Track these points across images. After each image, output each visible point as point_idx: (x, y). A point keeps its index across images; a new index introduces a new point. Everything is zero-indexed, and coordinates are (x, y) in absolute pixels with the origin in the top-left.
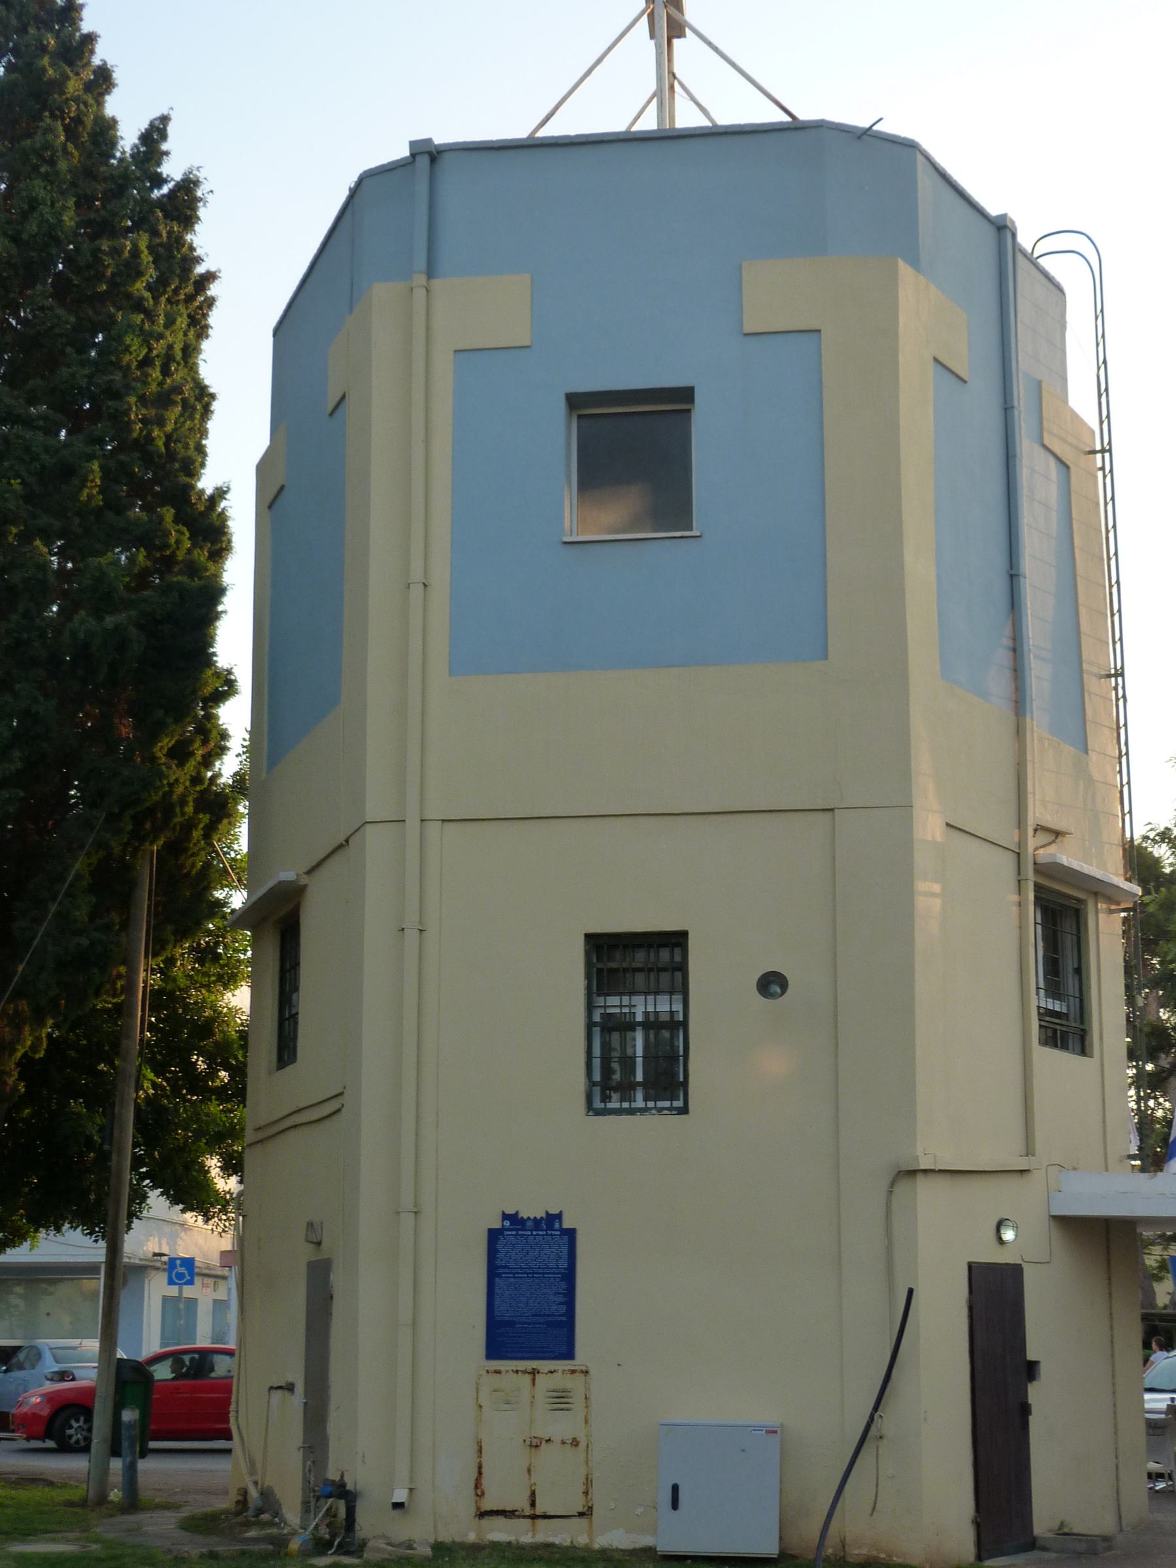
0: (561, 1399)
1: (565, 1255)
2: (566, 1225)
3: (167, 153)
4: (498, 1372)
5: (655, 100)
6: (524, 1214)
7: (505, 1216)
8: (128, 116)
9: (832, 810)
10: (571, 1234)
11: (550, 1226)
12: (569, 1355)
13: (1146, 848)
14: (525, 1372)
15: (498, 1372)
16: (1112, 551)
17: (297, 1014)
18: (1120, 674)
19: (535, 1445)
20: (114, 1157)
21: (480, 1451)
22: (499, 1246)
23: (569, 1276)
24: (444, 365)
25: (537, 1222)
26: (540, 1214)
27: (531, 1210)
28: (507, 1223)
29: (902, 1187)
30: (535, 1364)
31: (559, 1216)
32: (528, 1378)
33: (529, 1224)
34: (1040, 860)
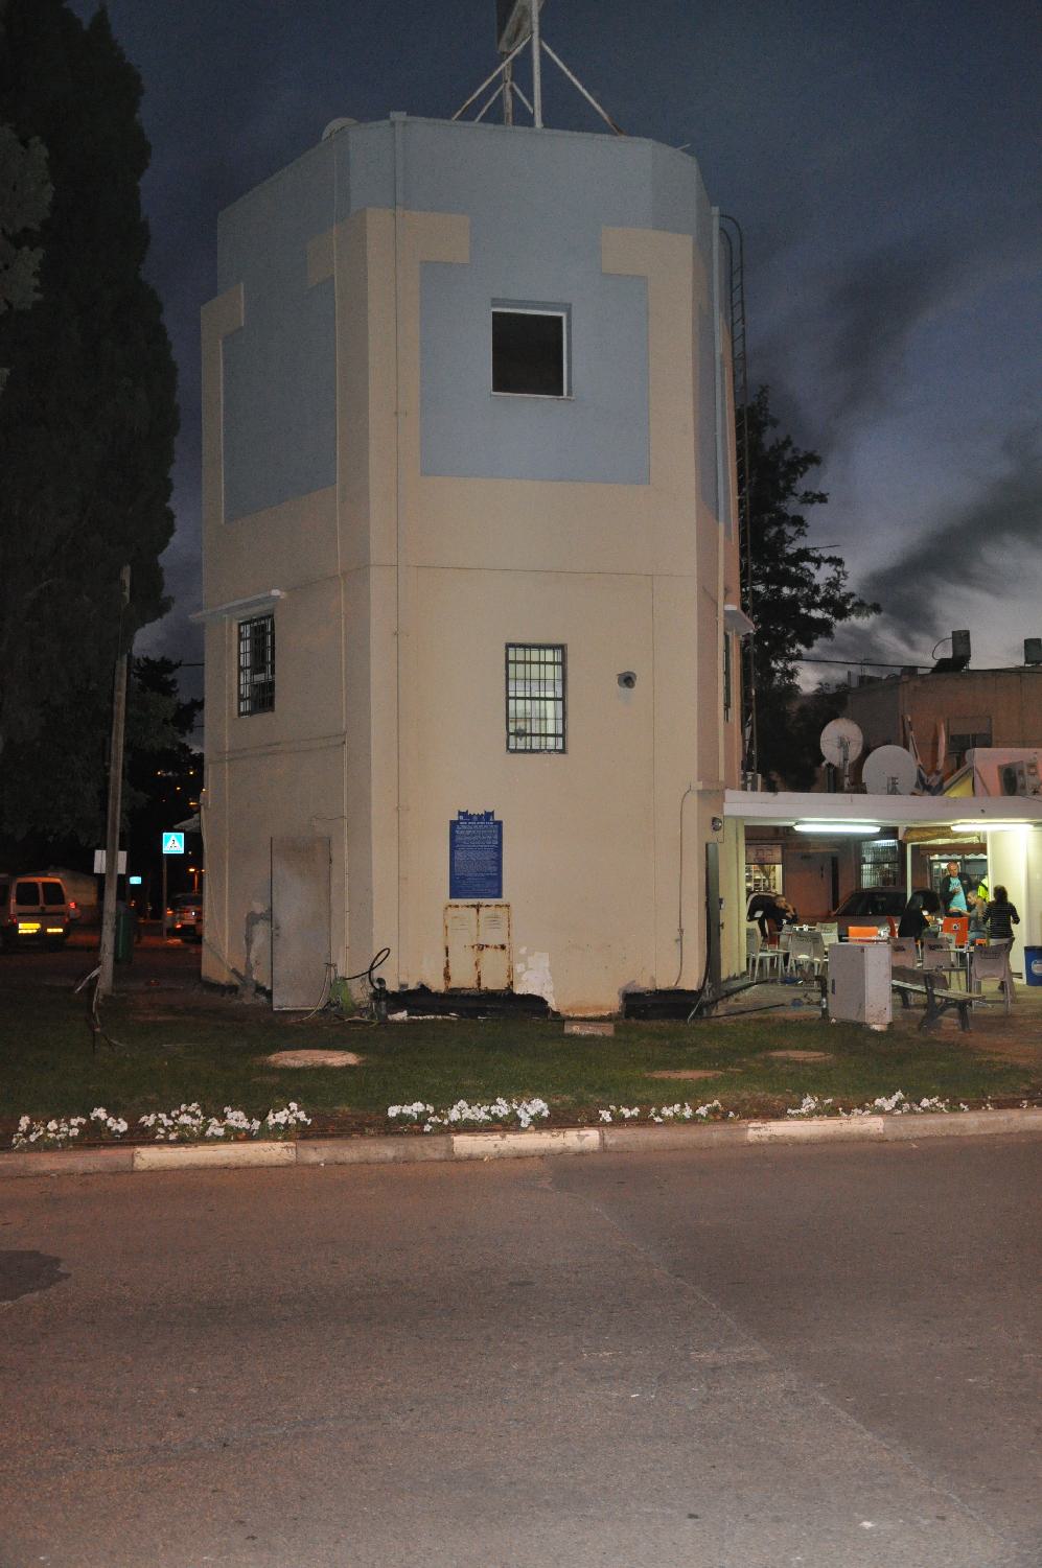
2: (497, 818)
3: (101, 22)
4: (457, 906)
6: (471, 812)
7: (460, 813)
10: (499, 824)
11: (488, 820)
12: (499, 895)
14: (473, 906)
15: (457, 906)
17: (199, 705)
18: (203, 664)
19: (481, 947)
20: (112, 769)
21: (447, 952)
23: (499, 849)
24: (861, 944)
25: (480, 817)
26: (481, 812)
27: (476, 809)
28: (461, 818)
30: (481, 901)
31: (492, 813)
32: (474, 910)
33: (475, 818)
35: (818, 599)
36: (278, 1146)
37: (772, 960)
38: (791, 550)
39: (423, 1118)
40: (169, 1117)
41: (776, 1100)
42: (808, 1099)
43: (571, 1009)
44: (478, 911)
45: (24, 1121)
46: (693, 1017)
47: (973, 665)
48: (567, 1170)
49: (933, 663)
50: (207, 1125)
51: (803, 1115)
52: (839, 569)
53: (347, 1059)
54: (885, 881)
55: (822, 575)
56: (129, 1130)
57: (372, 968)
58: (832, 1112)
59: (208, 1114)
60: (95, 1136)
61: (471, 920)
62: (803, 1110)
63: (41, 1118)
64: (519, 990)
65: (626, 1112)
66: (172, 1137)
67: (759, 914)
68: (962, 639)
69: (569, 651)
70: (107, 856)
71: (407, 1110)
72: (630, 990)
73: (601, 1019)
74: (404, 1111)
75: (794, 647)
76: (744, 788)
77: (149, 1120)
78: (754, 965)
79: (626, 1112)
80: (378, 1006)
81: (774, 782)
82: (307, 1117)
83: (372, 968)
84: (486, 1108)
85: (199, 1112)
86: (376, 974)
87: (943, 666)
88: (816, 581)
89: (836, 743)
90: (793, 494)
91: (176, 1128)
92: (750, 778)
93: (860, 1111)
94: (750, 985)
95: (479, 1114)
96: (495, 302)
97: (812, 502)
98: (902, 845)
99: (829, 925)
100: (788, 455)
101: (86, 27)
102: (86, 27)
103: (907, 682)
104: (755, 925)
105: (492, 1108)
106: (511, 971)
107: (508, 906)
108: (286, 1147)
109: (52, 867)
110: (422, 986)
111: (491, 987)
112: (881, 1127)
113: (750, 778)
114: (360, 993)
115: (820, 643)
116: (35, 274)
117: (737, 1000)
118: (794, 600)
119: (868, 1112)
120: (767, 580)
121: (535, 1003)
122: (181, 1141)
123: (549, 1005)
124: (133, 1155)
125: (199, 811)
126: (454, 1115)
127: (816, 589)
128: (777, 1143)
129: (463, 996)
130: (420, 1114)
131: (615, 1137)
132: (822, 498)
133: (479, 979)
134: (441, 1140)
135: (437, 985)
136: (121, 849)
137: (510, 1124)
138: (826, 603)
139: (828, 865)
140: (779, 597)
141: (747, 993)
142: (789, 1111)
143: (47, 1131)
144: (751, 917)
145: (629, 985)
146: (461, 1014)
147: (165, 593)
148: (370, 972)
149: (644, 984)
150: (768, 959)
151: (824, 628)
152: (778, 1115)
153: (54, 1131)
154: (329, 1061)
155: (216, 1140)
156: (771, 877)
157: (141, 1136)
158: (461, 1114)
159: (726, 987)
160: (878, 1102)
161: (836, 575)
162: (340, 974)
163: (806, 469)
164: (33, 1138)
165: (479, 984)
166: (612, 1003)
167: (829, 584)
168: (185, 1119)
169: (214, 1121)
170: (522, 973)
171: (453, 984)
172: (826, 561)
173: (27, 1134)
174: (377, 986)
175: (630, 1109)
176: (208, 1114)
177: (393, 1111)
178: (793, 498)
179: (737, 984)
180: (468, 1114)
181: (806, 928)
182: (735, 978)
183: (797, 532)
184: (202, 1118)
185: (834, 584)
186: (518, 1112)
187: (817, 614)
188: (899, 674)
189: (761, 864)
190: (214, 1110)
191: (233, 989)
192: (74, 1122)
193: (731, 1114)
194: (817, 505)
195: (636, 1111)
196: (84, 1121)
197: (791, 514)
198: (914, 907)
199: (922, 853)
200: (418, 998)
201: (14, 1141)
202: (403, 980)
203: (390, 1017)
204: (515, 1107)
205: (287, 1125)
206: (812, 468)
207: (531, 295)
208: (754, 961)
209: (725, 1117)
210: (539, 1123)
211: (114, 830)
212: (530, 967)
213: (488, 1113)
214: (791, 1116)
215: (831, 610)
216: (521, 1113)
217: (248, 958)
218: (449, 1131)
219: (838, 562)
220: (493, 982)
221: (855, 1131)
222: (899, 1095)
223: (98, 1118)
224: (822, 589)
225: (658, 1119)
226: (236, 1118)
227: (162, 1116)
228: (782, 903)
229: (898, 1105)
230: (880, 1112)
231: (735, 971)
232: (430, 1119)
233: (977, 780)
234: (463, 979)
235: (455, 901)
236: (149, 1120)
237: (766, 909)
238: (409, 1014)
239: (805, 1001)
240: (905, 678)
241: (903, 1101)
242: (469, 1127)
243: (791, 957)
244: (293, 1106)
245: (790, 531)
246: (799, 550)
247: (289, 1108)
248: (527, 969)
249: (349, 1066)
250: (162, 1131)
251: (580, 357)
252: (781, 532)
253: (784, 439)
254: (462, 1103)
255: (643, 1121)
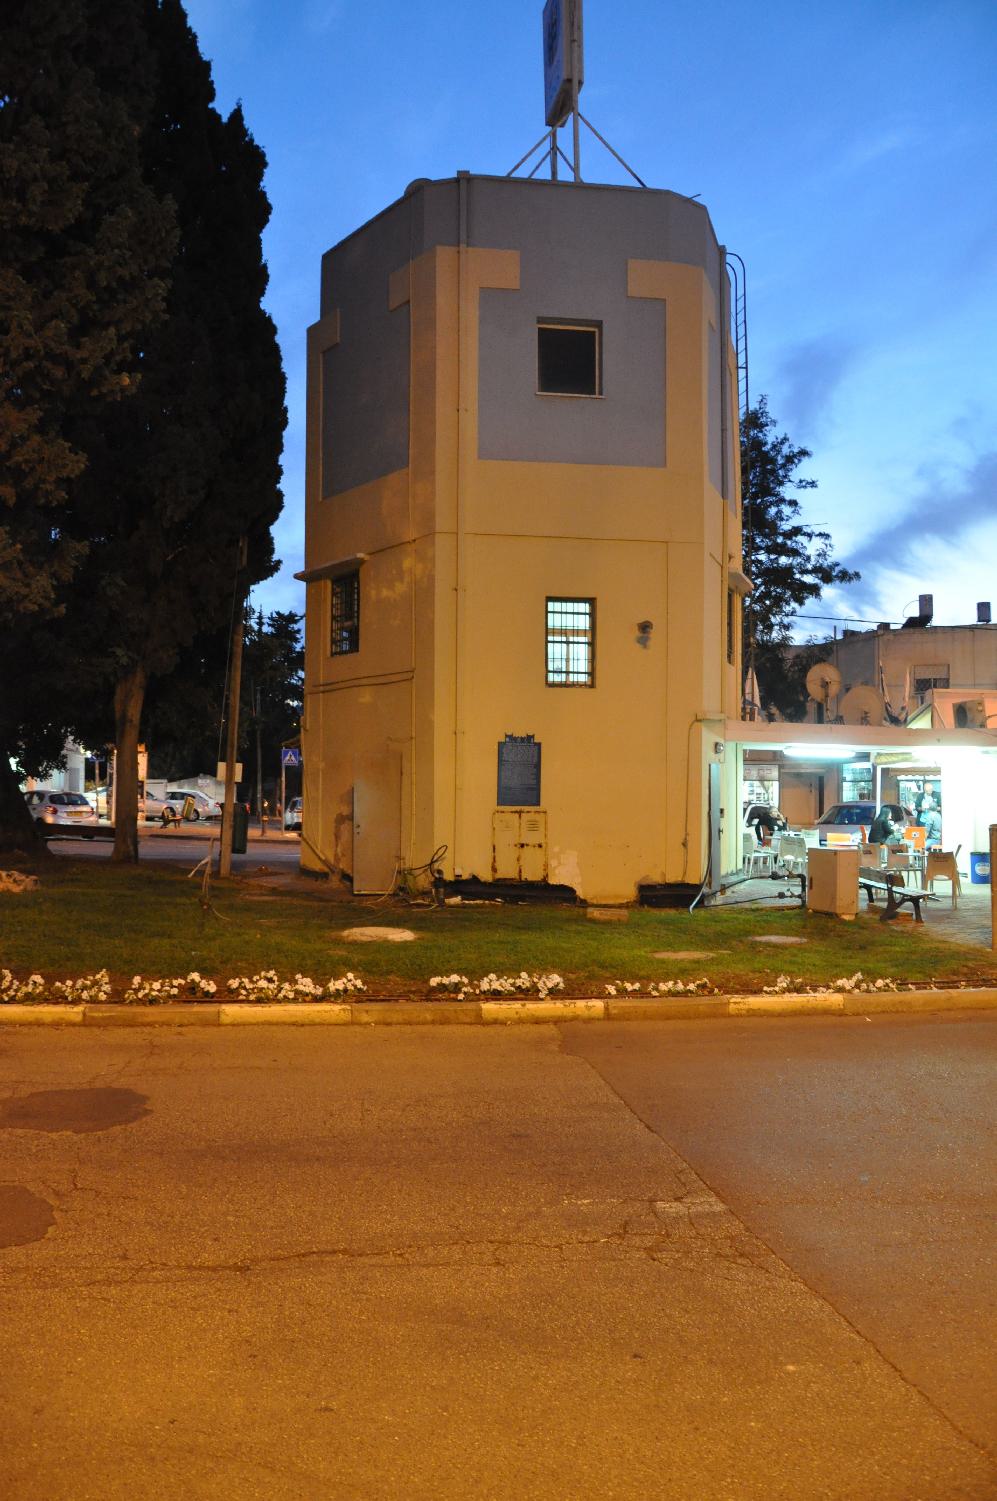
0: (533, 826)
1: (536, 755)
5: (549, 157)
6: (516, 735)
7: (507, 736)
8: (223, 107)
9: (667, 542)
10: (539, 745)
12: (538, 803)
13: (176, 212)
16: (740, 292)
22: (504, 750)
23: (538, 766)
26: (524, 735)
27: (520, 733)
28: (508, 739)
29: (696, 724)
30: (526, 808)
31: (533, 737)
32: (517, 815)
34: (731, 571)
35: (809, 567)
36: (337, 1008)
37: (765, 859)
38: (786, 526)
39: (457, 987)
40: (251, 981)
41: (755, 978)
42: (782, 978)
43: (595, 897)
44: (520, 816)
45: (137, 980)
46: (695, 907)
47: (936, 621)
48: (571, 1036)
49: (904, 621)
50: (280, 989)
51: (777, 993)
52: (827, 542)
53: (404, 935)
54: (862, 796)
55: (812, 548)
56: (217, 992)
57: (432, 862)
58: (799, 990)
59: (282, 980)
60: (191, 994)
61: (514, 823)
62: (777, 989)
63: (148, 977)
64: (552, 881)
65: (629, 987)
66: (252, 997)
67: (756, 821)
68: (926, 601)
69: (599, 604)
70: (227, 766)
71: (446, 981)
72: (644, 884)
73: (620, 906)
74: (444, 982)
75: (789, 605)
76: (743, 719)
77: (234, 983)
78: (749, 863)
79: (629, 987)
80: (437, 892)
81: (773, 715)
82: (363, 984)
83: (432, 862)
84: (511, 981)
85: (275, 978)
86: (436, 866)
87: (911, 623)
88: (807, 553)
89: (819, 683)
90: (790, 481)
91: (256, 991)
92: (748, 710)
93: (824, 990)
94: (745, 880)
95: (504, 984)
96: (540, 320)
97: (805, 487)
98: (875, 768)
99: (812, 832)
100: (785, 450)
101: (225, 119)
102: (225, 119)
103: (882, 635)
104: (752, 830)
105: (517, 981)
106: (546, 866)
107: (545, 812)
108: (344, 1010)
109: (201, 775)
110: (474, 876)
111: (530, 879)
112: (841, 1004)
113: (748, 710)
114: (424, 881)
115: (810, 601)
116: (164, 299)
117: (733, 892)
118: (789, 569)
119: (831, 991)
120: (769, 550)
121: (566, 893)
122: (259, 1001)
123: (578, 893)
124: (219, 1012)
125: (299, 732)
126: (485, 985)
127: (808, 558)
128: (753, 1013)
129: (507, 886)
130: (456, 984)
131: (618, 1005)
132: (813, 484)
133: (520, 871)
134: (471, 1006)
135: (486, 876)
136: (238, 762)
137: (529, 994)
138: (816, 570)
139: (816, 783)
140: (778, 564)
141: (742, 886)
142: (765, 988)
143: (152, 989)
144: (750, 824)
145: (644, 878)
146: (506, 900)
147: (275, 557)
148: (430, 865)
149: (656, 878)
150: (762, 860)
151: (814, 590)
152: (758, 992)
153: (159, 991)
154: (390, 937)
155: (286, 999)
156: (770, 791)
157: (229, 996)
158: (490, 985)
159: (724, 882)
160: (840, 982)
161: (824, 546)
162: (407, 866)
163: (800, 461)
164: (140, 995)
165: (520, 876)
166: (630, 893)
167: (819, 555)
168: (263, 984)
169: (286, 986)
170: (555, 868)
171: (499, 875)
172: (817, 535)
173: (136, 991)
174: (437, 876)
175: (632, 984)
176: (282, 980)
177: (434, 981)
178: (789, 484)
179: (734, 879)
180: (496, 985)
181: (792, 834)
182: (732, 874)
183: (793, 512)
184: (277, 983)
185: (822, 555)
186: (539, 985)
187: (809, 579)
188: (875, 629)
189: (762, 780)
190: (287, 977)
191: (324, 876)
192: (175, 983)
193: (716, 990)
194: (809, 489)
195: (637, 986)
196: (183, 982)
197: (787, 498)
198: (883, 818)
199: (892, 774)
200: (468, 887)
201: (126, 996)
202: (458, 872)
203: (447, 901)
204: (536, 980)
205: (346, 990)
206: (805, 460)
207: (571, 306)
208: (749, 859)
209: (711, 992)
210: (554, 993)
211: (232, 747)
212: (562, 861)
213: (512, 985)
214: (766, 992)
215: (820, 575)
216: (540, 985)
217: (336, 851)
218: (479, 1000)
219: (827, 536)
220: (532, 874)
221: (819, 1006)
222: (859, 975)
223: (193, 980)
224: (813, 559)
225: (655, 993)
226: (306, 984)
227: (246, 980)
228: (775, 813)
229: (857, 986)
230: (840, 990)
231: (732, 868)
232: (465, 989)
233: (935, 715)
234: (507, 871)
235: (502, 808)
236: (234, 983)
237: (762, 819)
238: (463, 899)
239: (789, 894)
240: (881, 632)
241: (862, 981)
242: (496, 995)
243: (779, 858)
244: (350, 975)
245: (786, 510)
246: (794, 527)
247: (346, 978)
248: (560, 864)
249: (406, 942)
250: (244, 992)
251: (612, 361)
252: (779, 512)
253: (782, 436)
254: (492, 976)
255: (642, 994)
